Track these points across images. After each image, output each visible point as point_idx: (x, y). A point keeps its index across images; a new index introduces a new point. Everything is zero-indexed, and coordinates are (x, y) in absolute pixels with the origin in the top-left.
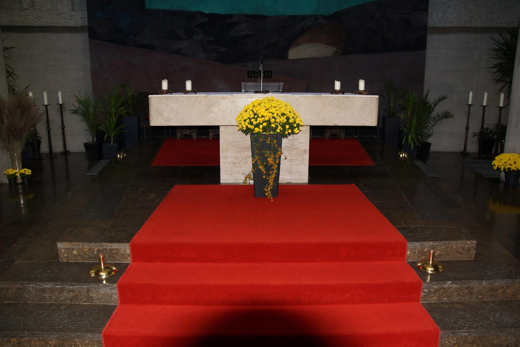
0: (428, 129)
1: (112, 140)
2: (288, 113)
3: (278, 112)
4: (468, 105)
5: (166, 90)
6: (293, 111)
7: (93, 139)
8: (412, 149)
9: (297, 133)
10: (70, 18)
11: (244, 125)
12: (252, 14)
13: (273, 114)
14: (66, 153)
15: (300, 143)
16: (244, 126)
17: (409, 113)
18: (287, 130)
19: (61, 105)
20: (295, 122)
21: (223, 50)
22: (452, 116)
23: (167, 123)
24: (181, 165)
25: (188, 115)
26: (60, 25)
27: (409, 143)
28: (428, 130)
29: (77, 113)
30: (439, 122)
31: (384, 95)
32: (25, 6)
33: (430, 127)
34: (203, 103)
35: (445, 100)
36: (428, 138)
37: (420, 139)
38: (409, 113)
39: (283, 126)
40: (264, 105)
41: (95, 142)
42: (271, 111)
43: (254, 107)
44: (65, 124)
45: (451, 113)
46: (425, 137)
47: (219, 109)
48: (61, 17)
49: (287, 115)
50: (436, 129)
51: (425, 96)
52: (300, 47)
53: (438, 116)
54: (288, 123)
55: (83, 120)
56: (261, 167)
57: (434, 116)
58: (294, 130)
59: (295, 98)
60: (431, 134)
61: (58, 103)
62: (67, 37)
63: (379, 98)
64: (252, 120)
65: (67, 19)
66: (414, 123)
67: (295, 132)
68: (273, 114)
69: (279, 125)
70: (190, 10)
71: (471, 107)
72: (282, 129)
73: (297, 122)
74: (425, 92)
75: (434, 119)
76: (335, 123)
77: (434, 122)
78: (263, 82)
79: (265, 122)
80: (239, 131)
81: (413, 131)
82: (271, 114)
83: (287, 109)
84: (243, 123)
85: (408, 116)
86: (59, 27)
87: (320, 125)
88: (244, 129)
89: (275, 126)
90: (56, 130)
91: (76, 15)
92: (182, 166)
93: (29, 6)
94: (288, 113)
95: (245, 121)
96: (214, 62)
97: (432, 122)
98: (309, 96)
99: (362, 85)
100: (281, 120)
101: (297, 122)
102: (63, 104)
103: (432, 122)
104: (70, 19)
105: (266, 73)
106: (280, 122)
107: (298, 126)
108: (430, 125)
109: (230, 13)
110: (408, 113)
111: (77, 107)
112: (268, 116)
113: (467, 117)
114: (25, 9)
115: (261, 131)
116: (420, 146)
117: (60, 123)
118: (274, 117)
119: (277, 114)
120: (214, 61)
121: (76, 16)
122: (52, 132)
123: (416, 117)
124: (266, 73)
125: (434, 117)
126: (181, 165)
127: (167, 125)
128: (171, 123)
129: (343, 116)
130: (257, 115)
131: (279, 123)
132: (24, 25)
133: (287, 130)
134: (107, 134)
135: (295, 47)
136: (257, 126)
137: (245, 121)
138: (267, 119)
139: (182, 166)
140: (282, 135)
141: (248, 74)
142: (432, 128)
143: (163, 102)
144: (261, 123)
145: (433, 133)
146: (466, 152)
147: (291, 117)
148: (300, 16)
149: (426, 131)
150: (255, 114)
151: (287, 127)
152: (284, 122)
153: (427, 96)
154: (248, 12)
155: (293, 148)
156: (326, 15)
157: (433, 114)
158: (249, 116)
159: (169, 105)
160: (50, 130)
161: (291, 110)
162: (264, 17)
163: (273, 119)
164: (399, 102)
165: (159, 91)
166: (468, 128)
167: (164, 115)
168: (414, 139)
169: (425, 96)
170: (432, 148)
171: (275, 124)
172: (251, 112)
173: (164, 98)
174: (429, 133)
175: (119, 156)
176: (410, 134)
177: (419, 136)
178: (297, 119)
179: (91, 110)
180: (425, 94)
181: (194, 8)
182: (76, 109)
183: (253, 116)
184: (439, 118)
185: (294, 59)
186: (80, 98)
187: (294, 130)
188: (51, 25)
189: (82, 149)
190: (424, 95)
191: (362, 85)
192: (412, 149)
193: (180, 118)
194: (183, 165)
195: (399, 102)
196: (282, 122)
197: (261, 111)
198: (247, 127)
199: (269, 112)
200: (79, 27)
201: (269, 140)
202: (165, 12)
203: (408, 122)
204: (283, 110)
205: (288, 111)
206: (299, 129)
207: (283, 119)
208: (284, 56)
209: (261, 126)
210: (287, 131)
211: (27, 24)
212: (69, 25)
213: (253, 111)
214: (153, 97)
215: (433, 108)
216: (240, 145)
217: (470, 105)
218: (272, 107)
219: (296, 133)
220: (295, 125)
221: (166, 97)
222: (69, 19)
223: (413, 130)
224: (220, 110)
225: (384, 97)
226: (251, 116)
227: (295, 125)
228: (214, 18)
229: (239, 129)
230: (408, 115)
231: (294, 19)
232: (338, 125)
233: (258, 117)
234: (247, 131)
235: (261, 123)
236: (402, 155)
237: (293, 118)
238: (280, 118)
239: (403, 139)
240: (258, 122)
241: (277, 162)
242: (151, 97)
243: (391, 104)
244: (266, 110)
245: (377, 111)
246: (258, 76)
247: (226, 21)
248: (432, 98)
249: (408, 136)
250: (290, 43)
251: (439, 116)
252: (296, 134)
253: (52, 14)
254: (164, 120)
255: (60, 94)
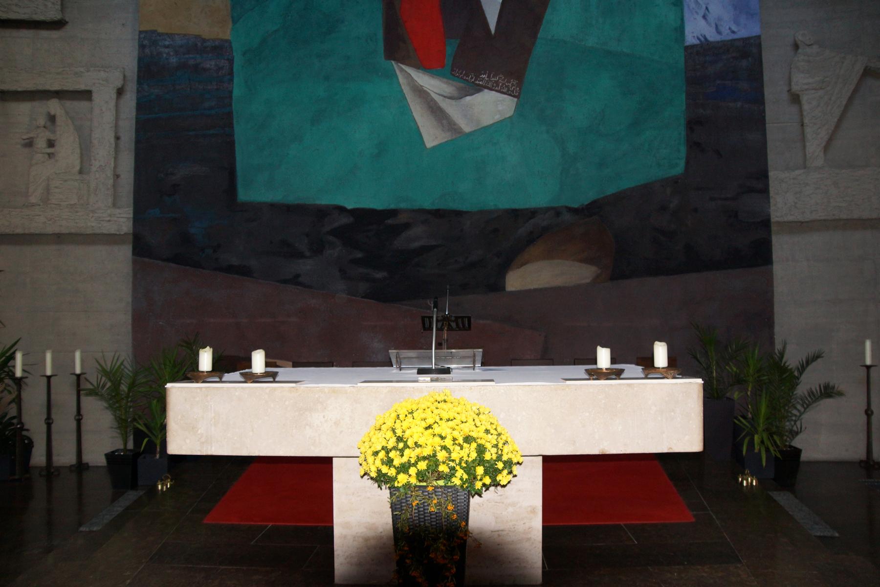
0: (792, 420)
1: (158, 450)
2: (482, 434)
3: (456, 434)
4: (864, 366)
5: (207, 372)
6: (496, 429)
7: (125, 444)
8: (764, 464)
9: (505, 484)
10: (108, 219)
11: (374, 465)
12: (434, 208)
13: (442, 438)
14: (81, 467)
15: (520, 490)
16: (374, 469)
17: (750, 389)
18: (479, 478)
19: (78, 376)
20: (499, 458)
21: (379, 275)
22: (840, 394)
23: (205, 448)
24: (265, 524)
25: (253, 431)
26: (89, 231)
27: (756, 451)
28: (793, 423)
29: (96, 394)
30: (814, 405)
31: (698, 356)
32: (33, 200)
33: (796, 416)
34: (287, 403)
35: (819, 360)
36: (794, 438)
37: (778, 442)
38: (750, 389)
39: (469, 469)
40: (423, 416)
41: (130, 450)
42: (437, 430)
43: (397, 421)
44: (83, 412)
45: (838, 388)
46: (788, 437)
47: (324, 417)
48: (93, 217)
49: (479, 441)
50: (809, 417)
51: (780, 353)
52: (529, 268)
53: (811, 393)
54: (480, 461)
55: (107, 408)
56: (413, 573)
57: (804, 394)
58: (499, 478)
59: (502, 391)
60: (799, 430)
61: (73, 372)
62: (100, 251)
63: (704, 384)
64: (392, 454)
65: (103, 221)
66: (763, 409)
67: (500, 480)
68: (442, 438)
69: (458, 468)
70: (318, 202)
71: (872, 369)
72: (465, 476)
73: (505, 458)
74: (778, 346)
75: (802, 400)
76: (602, 447)
77: (803, 406)
78: (435, 349)
79: (424, 458)
80: (362, 477)
81: (761, 424)
82: (438, 439)
83: (478, 424)
84: (370, 459)
85: (748, 395)
86: (87, 235)
87: (565, 454)
88: (374, 475)
89: (448, 470)
90: (64, 423)
91: (120, 214)
92: (267, 526)
93: (40, 200)
94: (482, 434)
95: (376, 453)
96: (363, 299)
97: (799, 407)
98: (536, 386)
99: (661, 354)
100: (464, 453)
101: (505, 458)
102: (82, 374)
103: (799, 407)
104: (109, 221)
105: (460, 321)
106: (461, 459)
107: (509, 464)
108: (795, 412)
109: (392, 206)
110: (748, 390)
111: (95, 384)
112: (429, 444)
113: (865, 389)
114: (33, 205)
115: (413, 481)
116: (779, 455)
117: (74, 409)
118: (444, 448)
119: (454, 439)
120: (362, 297)
121: (119, 216)
122: (54, 427)
123: (766, 398)
124: (460, 321)
125: (803, 395)
126: (265, 524)
127: (204, 454)
128: (213, 448)
129: (620, 430)
130: (405, 440)
131: (457, 462)
132: (27, 232)
133: (479, 478)
134: (148, 436)
135: (518, 268)
136: (404, 468)
137: (376, 453)
138: (427, 452)
139: (267, 526)
140: (469, 491)
141: (424, 324)
142: (801, 418)
143: (197, 399)
144: (413, 461)
145: (803, 429)
146: (874, 461)
147: (488, 446)
148: (527, 209)
149: (788, 423)
150: (399, 439)
151: (480, 470)
152: (470, 460)
153: (782, 355)
154: (427, 205)
155: (503, 503)
156: (576, 206)
157: (802, 390)
158: (384, 444)
159: (211, 407)
160: (52, 423)
161: (489, 428)
162: (459, 213)
163: (443, 451)
164: (727, 367)
165: (190, 373)
166: (870, 412)
167: (198, 430)
168: (766, 444)
169: (778, 354)
170: (804, 457)
171: (448, 464)
172: (390, 434)
173: (199, 390)
174: (795, 428)
175: (160, 487)
176: (757, 434)
177: (775, 437)
178: (506, 449)
179: (124, 388)
180: (778, 350)
181: (325, 200)
182: (91, 387)
183: (395, 444)
184: (813, 398)
185: (518, 291)
186: (104, 366)
187: (499, 478)
188: (73, 231)
189: (102, 461)
190: (776, 351)
191: (661, 354)
192: (764, 464)
193: (235, 438)
194: (271, 524)
195: (727, 367)
196: (465, 458)
197: (415, 432)
198: (379, 471)
199: (434, 435)
200: (122, 235)
201: (435, 504)
202: (273, 206)
203: (750, 407)
204: (467, 429)
205: (482, 428)
206: (510, 473)
207: (470, 453)
208: (497, 286)
209: (413, 471)
210: (481, 480)
211: (32, 231)
212: (105, 232)
213: (394, 431)
214: (175, 387)
215: (798, 378)
216: (379, 496)
217: (868, 367)
218: (441, 419)
219: (502, 483)
220: (500, 465)
221: (204, 389)
222: (106, 221)
223: (761, 425)
224: (326, 421)
225: (698, 361)
226: (389, 442)
227: (500, 465)
228: (363, 216)
229: (362, 473)
230: (749, 393)
231: (515, 214)
232: (608, 453)
233: (406, 446)
234: (381, 479)
235: (413, 461)
236: (747, 480)
237: (496, 446)
238: (462, 449)
239: (743, 445)
240: (405, 459)
241: (457, 557)
242: (172, 387)
243: (712, 373)
244: (427, 428)
245: (702, 414)
246: (443, 327)
247: (386, 221)
248: (792, 359)
249: (754, 436)
250: (507, 262)
251: (812, 393)
252: (504, 486)
253: (77, 212)
254: (198, 441)
255: (78, 355)
